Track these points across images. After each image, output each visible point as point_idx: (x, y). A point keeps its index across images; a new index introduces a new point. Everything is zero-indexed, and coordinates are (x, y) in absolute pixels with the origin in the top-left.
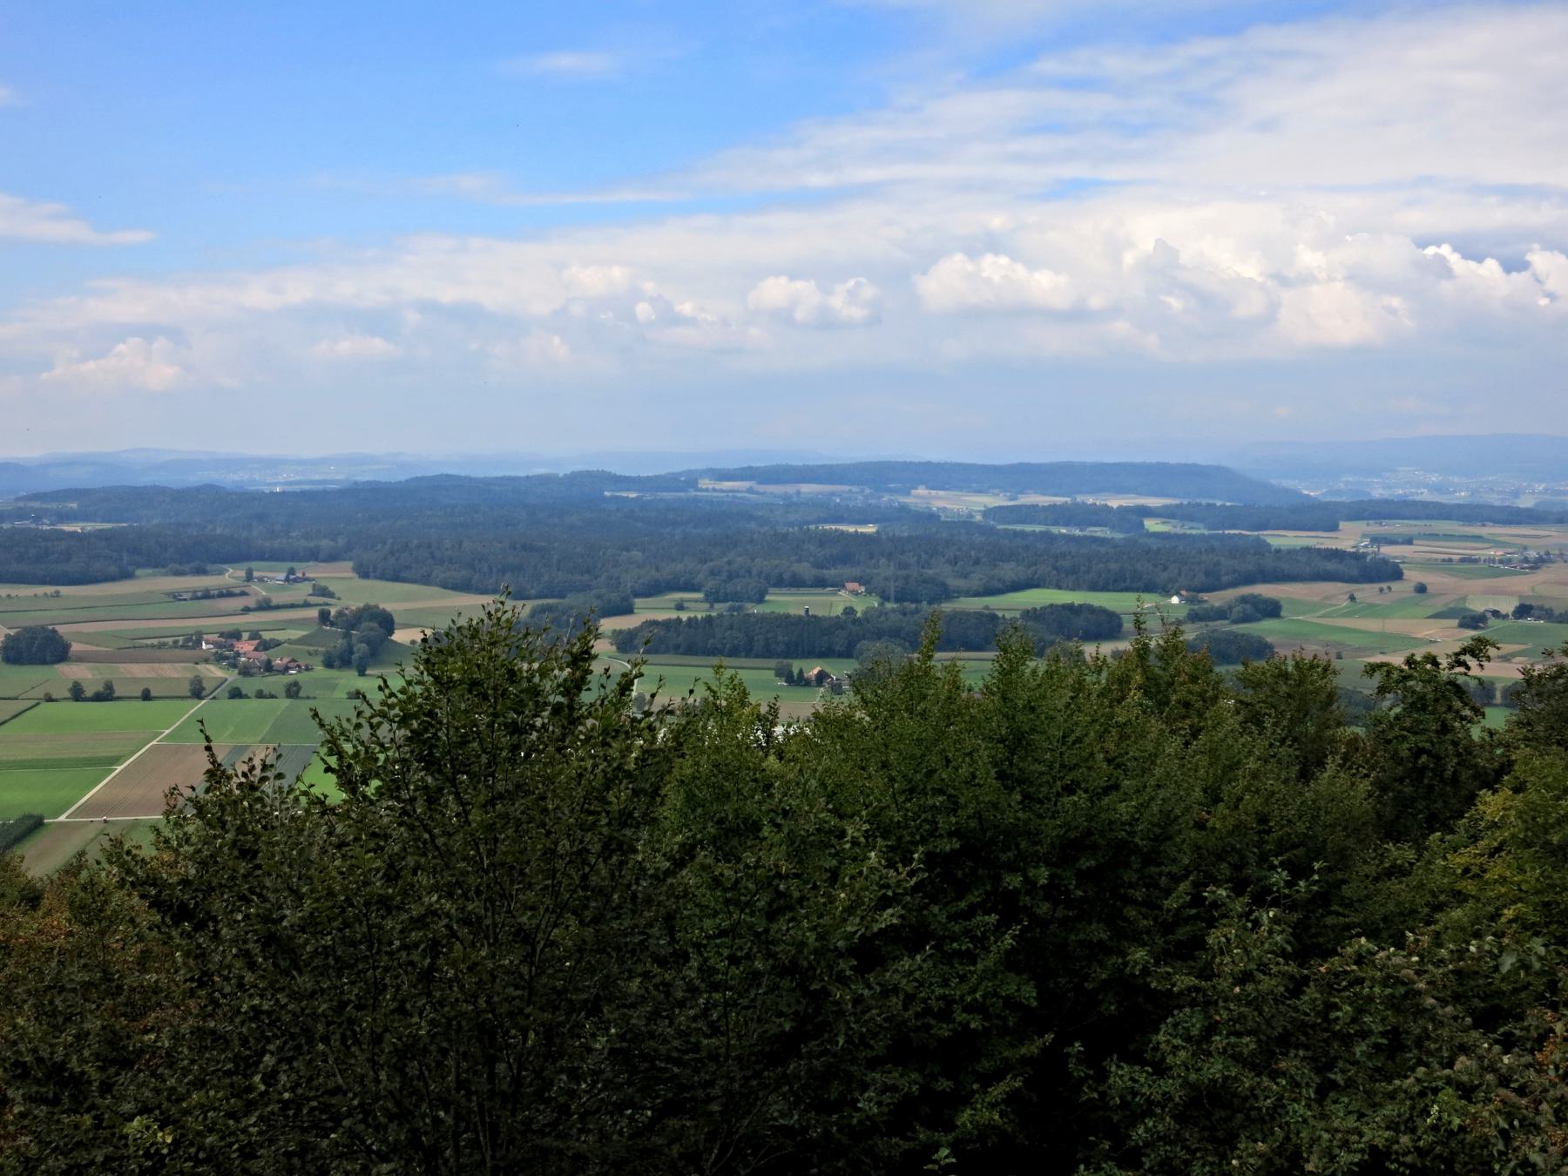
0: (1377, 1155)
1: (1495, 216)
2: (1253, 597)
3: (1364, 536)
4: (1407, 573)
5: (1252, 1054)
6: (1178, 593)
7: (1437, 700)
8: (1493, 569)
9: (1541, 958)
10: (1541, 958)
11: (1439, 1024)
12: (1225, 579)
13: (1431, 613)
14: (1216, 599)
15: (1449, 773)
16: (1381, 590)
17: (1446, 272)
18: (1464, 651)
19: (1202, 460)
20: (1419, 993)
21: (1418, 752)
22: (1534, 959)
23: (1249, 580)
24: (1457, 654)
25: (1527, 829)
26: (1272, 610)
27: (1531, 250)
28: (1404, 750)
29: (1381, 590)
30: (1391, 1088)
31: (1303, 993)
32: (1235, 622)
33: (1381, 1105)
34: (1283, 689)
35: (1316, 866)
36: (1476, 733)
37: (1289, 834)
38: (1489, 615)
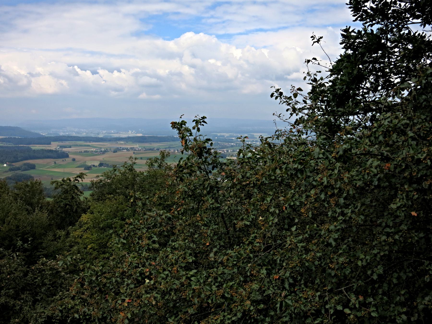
0: (50, 318)
1: (88, 60)
2: (27, 163)
3: (58, 146)
4: (70, 156)
5: (13, 294)
6: (6, 163)
7: (71, 190)
8: (93, 154)
9: (69, 262)
10: (69, 262)
11: (65, 279)
12: (19, 159)
13: (79, 165)
14: (17, 165)
15: (74, 210)
16: (63, 160)
17: (77, 74)
18: (77, 177)
19: (12, 125)
20: (60, 272)
21: (66, 205)
22: (68, 262)
23: (26, 159)
24: (76, 178)
25: (93, 224)
26: (33, 167)
27: (99, 69)
28: (62, 205)
29: (63, 160)
30: (53, 299)
31: (28, 275)
32: (22, 171)
33: (51, 304)
34: (27, 189)
35: (30, 239)
36: (82, 198)
37: (25, 231)
38: (92, 166)
